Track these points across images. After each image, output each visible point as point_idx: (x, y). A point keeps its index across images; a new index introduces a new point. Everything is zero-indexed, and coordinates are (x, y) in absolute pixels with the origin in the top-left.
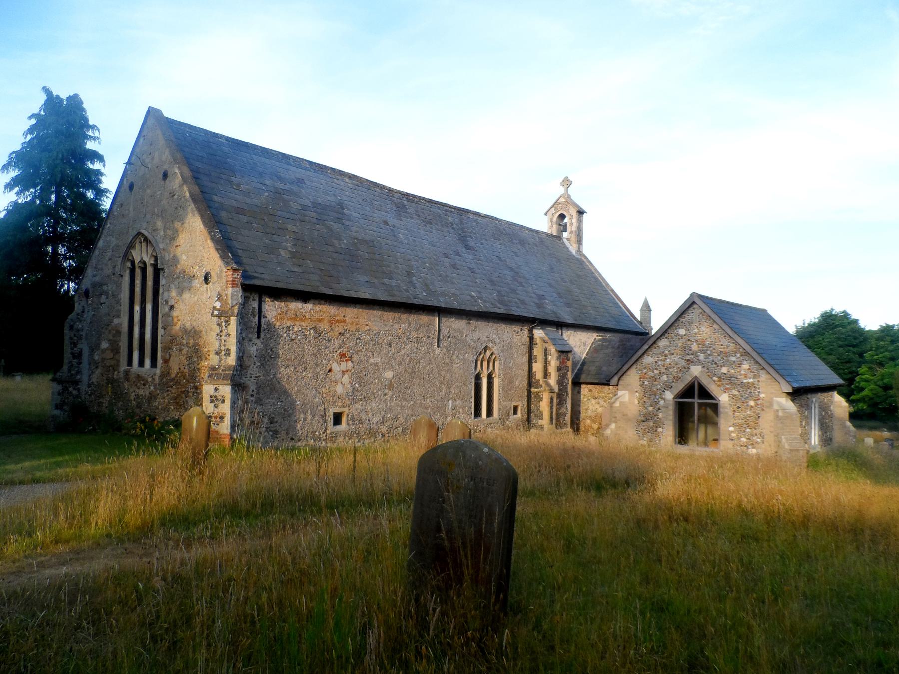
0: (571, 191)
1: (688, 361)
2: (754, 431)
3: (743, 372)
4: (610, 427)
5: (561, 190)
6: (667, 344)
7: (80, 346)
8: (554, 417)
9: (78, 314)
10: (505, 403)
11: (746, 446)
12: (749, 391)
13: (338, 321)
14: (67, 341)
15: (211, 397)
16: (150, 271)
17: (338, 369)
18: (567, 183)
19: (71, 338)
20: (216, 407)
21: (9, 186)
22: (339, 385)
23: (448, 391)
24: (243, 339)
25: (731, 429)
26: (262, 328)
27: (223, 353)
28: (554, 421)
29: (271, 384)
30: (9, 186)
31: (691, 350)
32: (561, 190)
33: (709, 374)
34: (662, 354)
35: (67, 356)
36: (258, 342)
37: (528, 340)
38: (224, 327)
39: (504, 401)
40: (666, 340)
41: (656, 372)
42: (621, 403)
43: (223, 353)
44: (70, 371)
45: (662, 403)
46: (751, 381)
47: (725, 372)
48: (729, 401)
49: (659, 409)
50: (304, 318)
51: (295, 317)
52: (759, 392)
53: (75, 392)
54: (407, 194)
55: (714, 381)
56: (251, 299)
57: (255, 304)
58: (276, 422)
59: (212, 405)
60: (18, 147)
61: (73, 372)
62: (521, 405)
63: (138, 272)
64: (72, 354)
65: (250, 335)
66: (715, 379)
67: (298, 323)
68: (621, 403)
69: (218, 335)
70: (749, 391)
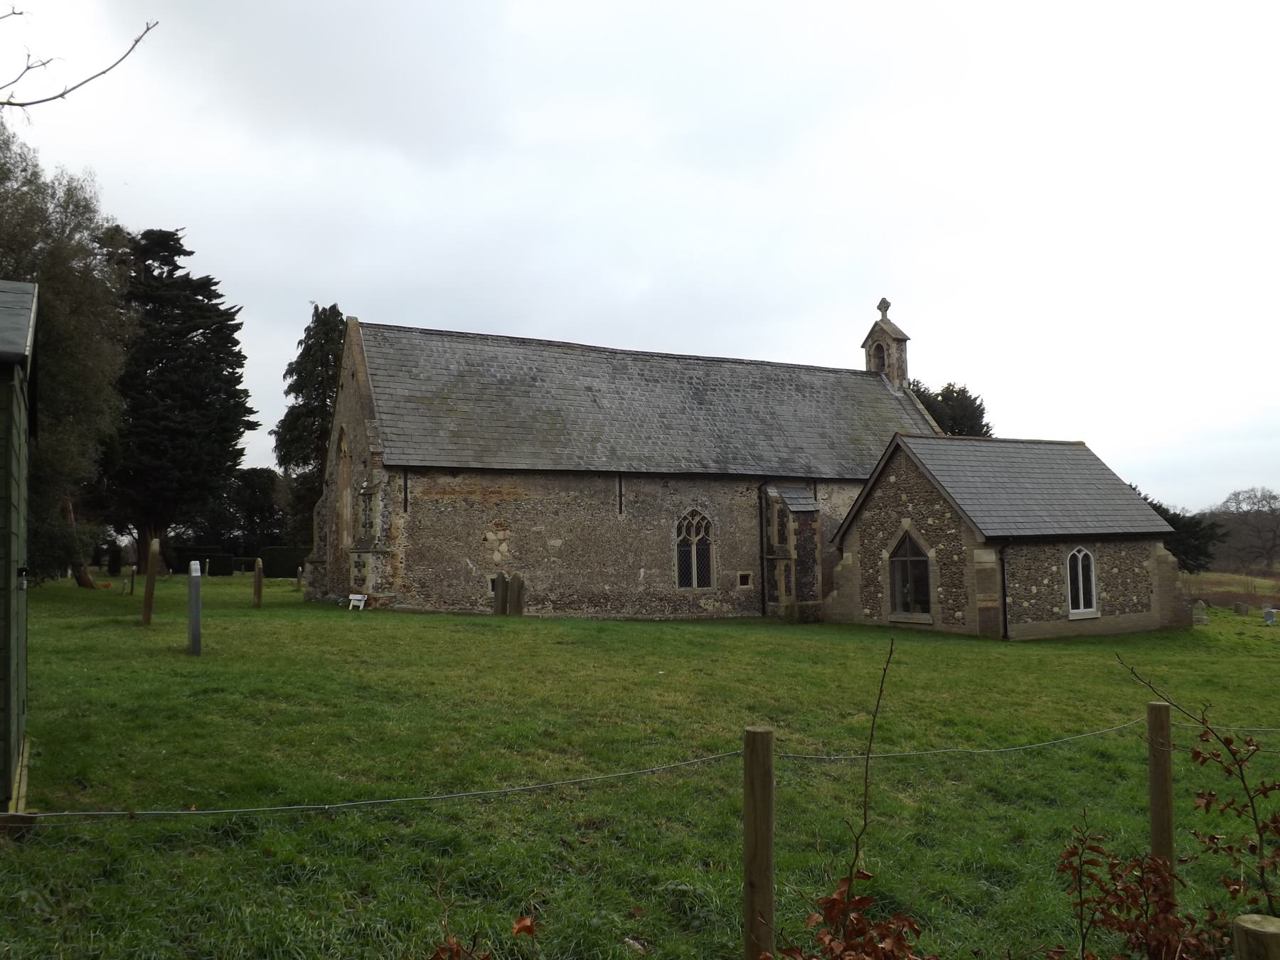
0: (891, 315)
2: (959, 591)
4: (831, 594)
5: (878, 316)
7: (325, 530)
10: (724, 572)
11: (953, 609)
13: (491, 492)
14: (315, 527)
18: (884, 306)
19: (318, 523)
20: (359, 571)
21: (287, 393)
22: (496, 552)
25: (940, 589)
28: (793, 592)
30: (287, 393)
32: (878, 316)
34: (877, 506)
35: (316, 539)
39: (723, 570)
42: (843, 566)
44: (318, 552)
46: (953, 531)
47: (931, 523)
48: (937, 556)
50: (453, 492)
51: (444, 492)
53: (322, 571)
55: (922, 534)
57: (401, 482)
60: (294, 359)
64: (320, 537)
66: (923, 531)
67: (446, 497)
68: (843, 566)
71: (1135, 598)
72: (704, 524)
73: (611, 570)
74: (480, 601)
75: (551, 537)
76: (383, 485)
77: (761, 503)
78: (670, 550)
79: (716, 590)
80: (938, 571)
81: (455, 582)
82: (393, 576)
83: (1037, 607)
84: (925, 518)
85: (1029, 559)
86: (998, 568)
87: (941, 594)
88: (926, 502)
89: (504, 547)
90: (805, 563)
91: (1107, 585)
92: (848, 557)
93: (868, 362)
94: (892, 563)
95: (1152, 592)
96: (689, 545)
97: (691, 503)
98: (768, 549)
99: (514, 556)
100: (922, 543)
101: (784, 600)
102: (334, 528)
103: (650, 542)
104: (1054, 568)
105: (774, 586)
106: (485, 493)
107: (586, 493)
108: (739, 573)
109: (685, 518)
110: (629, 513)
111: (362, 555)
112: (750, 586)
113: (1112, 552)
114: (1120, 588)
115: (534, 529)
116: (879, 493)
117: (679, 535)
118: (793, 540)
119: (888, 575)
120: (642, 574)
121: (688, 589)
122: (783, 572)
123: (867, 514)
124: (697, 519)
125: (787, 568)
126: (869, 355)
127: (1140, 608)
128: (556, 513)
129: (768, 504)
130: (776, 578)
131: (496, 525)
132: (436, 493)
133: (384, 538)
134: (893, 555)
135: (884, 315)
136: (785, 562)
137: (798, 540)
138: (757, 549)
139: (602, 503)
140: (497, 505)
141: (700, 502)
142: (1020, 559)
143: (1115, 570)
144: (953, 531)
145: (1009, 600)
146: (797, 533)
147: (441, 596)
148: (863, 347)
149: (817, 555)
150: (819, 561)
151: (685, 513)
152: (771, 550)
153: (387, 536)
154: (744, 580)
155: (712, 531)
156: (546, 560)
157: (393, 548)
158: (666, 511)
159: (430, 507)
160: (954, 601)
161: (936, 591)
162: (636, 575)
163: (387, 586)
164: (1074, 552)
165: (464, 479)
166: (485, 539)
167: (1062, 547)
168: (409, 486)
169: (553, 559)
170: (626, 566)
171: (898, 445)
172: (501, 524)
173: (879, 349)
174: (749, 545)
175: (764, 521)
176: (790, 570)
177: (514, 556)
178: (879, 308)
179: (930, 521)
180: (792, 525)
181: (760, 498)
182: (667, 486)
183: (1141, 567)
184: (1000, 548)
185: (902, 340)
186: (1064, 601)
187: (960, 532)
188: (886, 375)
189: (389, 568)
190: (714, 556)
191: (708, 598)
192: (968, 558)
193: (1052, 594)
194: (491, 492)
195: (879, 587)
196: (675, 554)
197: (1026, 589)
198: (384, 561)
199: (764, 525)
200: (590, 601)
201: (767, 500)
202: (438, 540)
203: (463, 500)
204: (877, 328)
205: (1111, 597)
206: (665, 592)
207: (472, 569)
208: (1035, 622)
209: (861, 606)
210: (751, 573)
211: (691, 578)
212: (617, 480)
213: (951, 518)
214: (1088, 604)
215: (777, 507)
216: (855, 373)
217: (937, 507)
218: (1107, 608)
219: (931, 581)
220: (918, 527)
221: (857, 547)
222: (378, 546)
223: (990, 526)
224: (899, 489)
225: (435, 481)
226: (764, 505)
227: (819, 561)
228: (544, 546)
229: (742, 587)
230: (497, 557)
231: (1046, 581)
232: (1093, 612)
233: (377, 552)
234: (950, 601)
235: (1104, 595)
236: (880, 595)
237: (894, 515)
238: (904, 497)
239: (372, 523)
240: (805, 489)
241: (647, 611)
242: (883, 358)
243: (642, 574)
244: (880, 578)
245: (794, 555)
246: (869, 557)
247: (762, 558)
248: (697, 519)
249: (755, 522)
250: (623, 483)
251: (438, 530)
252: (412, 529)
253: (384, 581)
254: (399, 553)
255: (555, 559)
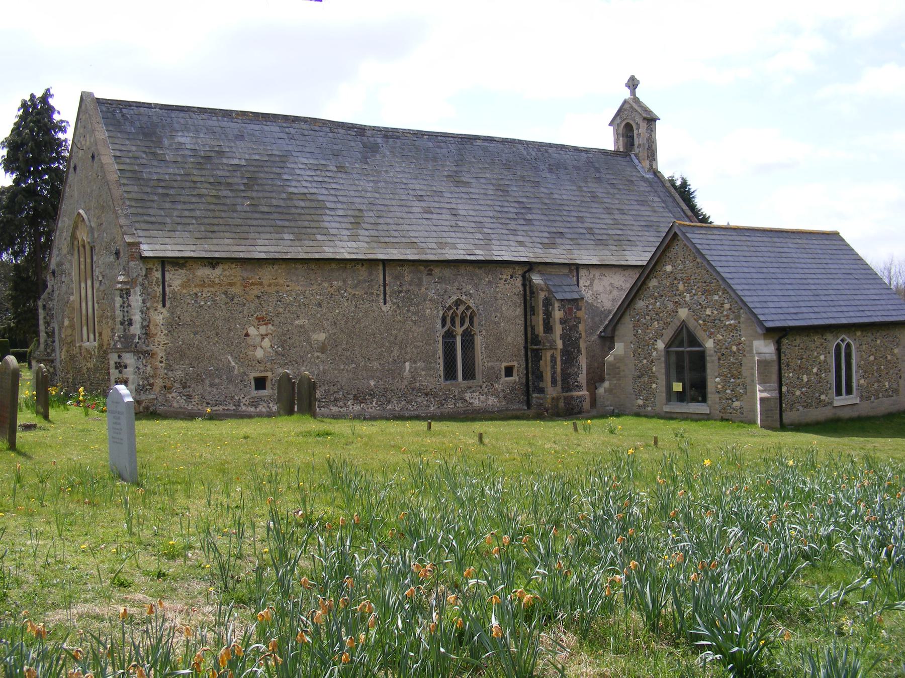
0: (639, 92)
1: (676, 302)
2: (738, 381)
3: (725, 313)
5: (626, 94)
6: (656, 284)
7: (52, 325)
8: (559, 379)
9: (49, 294)
11: (731, 399)
12: (732, 334)
13: (252, 284)
14: (41, 322)
15: (116, 363)
16: (88, 247)
17: (256, 333)
18: (633, 84)
19: (45, 318)
20: (120, 372)
22: (259, 349)
23: (403, 352)
24: (148, 309)
25: (718, 380)
26: (167, 297)
27: (126, 323)
28: (559, 383)
29: (181, 351)
31: (678, 290)
32: (626, 94)
33: (695, 317)
35: (43, 335)
36: (164, 310)
37: (521, 289)
38: (125, 300)
39: (488, 362)
40: (655, 279)
41: (648, 318)
43: (126, 323)
44: (45, 349)
45: (654, 353)
46: (732, 322)
47: (710, 314)
48: (715, 347)
49: (652, 362)
51: (203, 284)
52: (740, 335)
54: (386, 130)
56: (154, 270)
57: (158, 275)
58: (189, 387)
59: (117, 370)
61: (49, 351)
62: (516, 365)
63: (81, 248)
64: (47, 333)
65: (155, 305)
66: (701, 322)
67: (206, 290)
69: (121, 306)
70: (732, 334)
71: (887, 384)
72: (468, 314)
73: (376, 364)
74: (244, 400)
75: (314, 331)
76: (140, 279)
77: (525, 290)
78: (436, 342)
79: (481, 383)
80: (716, 362)
81: (217, 381)
82: (153, 377)
83: (808, 395)
84: (704, 308)
85: (802, 349)
86: (775, 357)
87: (719, 383)
88: (704, 292)
89: (266, 343)
90: (570, 354)
91: (865, 372)
92: (619, 348)
93: (616, 141)
94: (667, 352)
95: (900, 377)
96: (454, 337)
97: (456, 291)
98: (532, 338)
99: (276, 352)
100: (700, 335)
101: (552, 392)
102: (66, 323)
103: (416, 334)
104: (822, 357)
105: (540, 377)
106: (246, 284)
107: (350, 282)
108: (504, 364)
109: (450, 308)
110: (394, 303)
111: (123, 355)
112: (515, 378)
113: (869, 340)
114: (875, 374)
115: (297, 322)
116: (653, 283)
117: (443, 326)
118: (558, 330)
119: (663, 365)
120: (408, 368)
121: (454, 382)
122: (549, 363)
123: (640, 304)
124: (462, 308)
125: (553, 358)
126: (618, 134)
127: (891, 393)
128: (320, 305)
129: (532, 293)
130: (541, 369)
131: (258, 319)
132: (195, 286)
133: (144, 336)
134: (668, 346)
135: (633, 93)
136: (552, 351)
137: (563, 330)
138: (521, 340)
139: (366, 293)
140: (258, 297)
141: (464, 290)
142: (793, 347)
143: (872, 358)
144: (732, 322)
145: (784, 389)
146: (563, 322)
147: (203, 397)
148: (610, 124)
149: (583, 345)
150: (584, 351)
151: (450, 302)
152: (535, 340)
153: (146, 334)
154: (509, 371)
155: (476, 320)
156: (309, 355)
157: (151, 347)
158: (430, 300)
159: (189, 301)
160: (732, 391)
161: (714, 381)
162: (402, 369)
163: (148, 387)
164: (839, 341)
165: (224, 270)
166: (247, 335)
167: (829, 336)
168: (167, 279)
169: (316, 354)
170: (391, 360)
171: (675, 234)
172: (263, 318)
173: (629, 127)
174: (515, 336)
175: (529, 309)
176: (556, 362)
177: (276, 352)
178: (628, 85)
179: (708, 312)
180: (558, 314)
181: (524, 285)
182: (431, 275)
183: (893, 355)
184: (777, 338)
185: (651, 120)
186: (830, 389)
187: (739, 322)
188: (636, 155)
189: (149, 368)
190: (479, 347)
191: (473, 392)
192: (747, 349)
193: (820, 382)
194: (252, 284)
195: (653, 378)
196: (440, 347)
197: (798, 378)
198: (144, 361)
199: (529, 313)
200: (355, 398)
201: (531, 287)
202: (198, 336)
203: (224, 293)
204: (626, 106)
205: (868, 384)
206: (431, 386)
207: (234, 367)
208: (805, 410)
209: (634, 396)
210: (515, 364)
211: (456, 371)
212: (381, 268)
213: (730, 309)
214: (849, 391)
215: (542, 295)
216: (604, 152)
217: (716, 297)
218: (865, 394)
219: (709, 371)
220: (695, 317)
221: (630, 337)
222: (138, 345)
223: (769, 318)
224: (675, 279)
225: (194, 274)
226: (528, 293)
227: (584, 351)
228: (308, 340)
229: (507, 379)
230: (259, 353)
231: (815, 370)
232: (854, 399)
233: (138, 352)
234: (728, 391)
235: (862, 381)
236: (654, 386)
237: (670, 306)
238: (681, 287)
239: (131, 320)
240: (568, 275)
241: (413, 406)
242: (632, 137)
243: (408, 368)
244: (654, 369)
245: (560, 344)
246: (642, 347)
247: (526, 348)
248: (462, 308)
249: (519, 311)
250: (387, 272)
251: (198, 326)
252: (172, 326)
253: (146, 382)
254: (159, 352)
255: (319, 354)
